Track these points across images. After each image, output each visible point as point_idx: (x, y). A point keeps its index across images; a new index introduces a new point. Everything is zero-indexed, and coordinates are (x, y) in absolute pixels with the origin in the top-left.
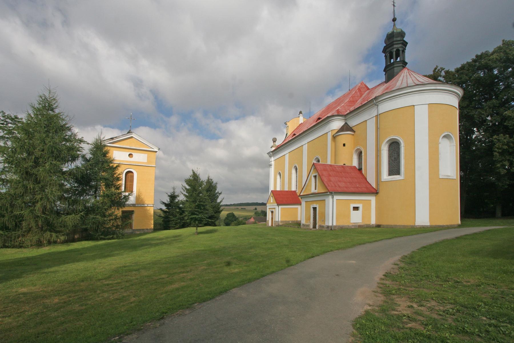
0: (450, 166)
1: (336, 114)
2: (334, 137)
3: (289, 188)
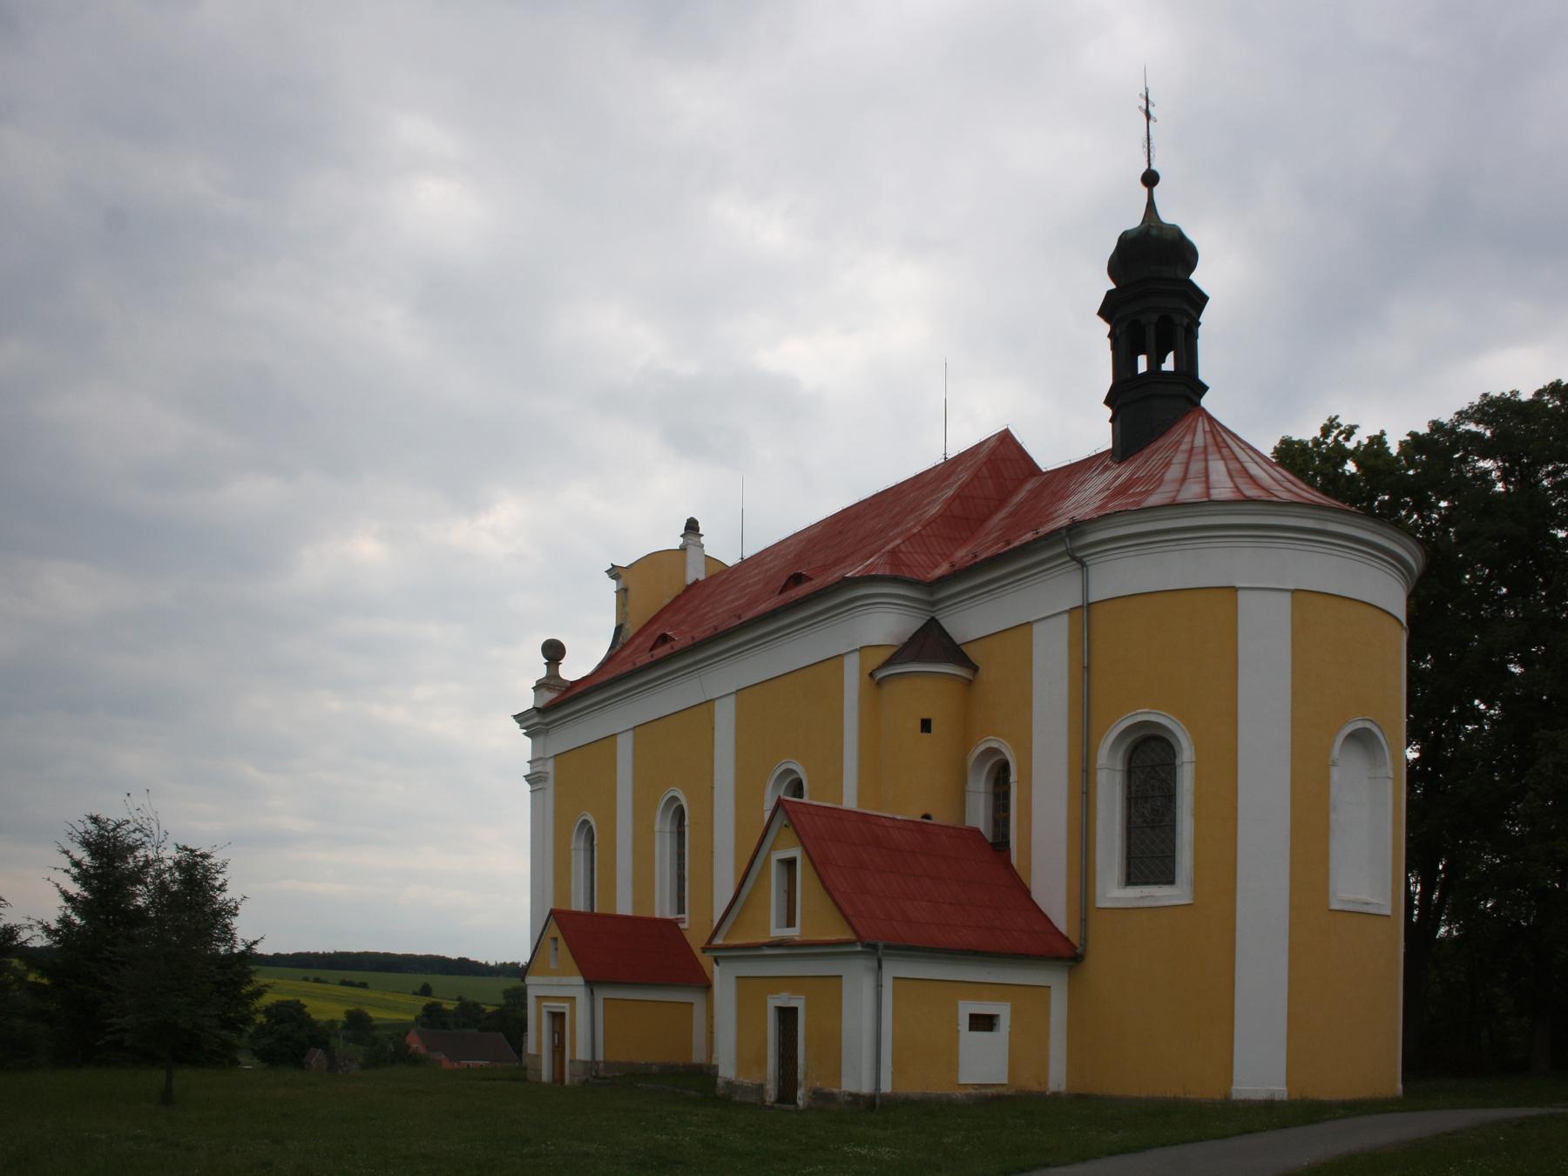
0: (1368, 867)
1: (885, 570)
2: (875, 681)
3: (636, 903)
